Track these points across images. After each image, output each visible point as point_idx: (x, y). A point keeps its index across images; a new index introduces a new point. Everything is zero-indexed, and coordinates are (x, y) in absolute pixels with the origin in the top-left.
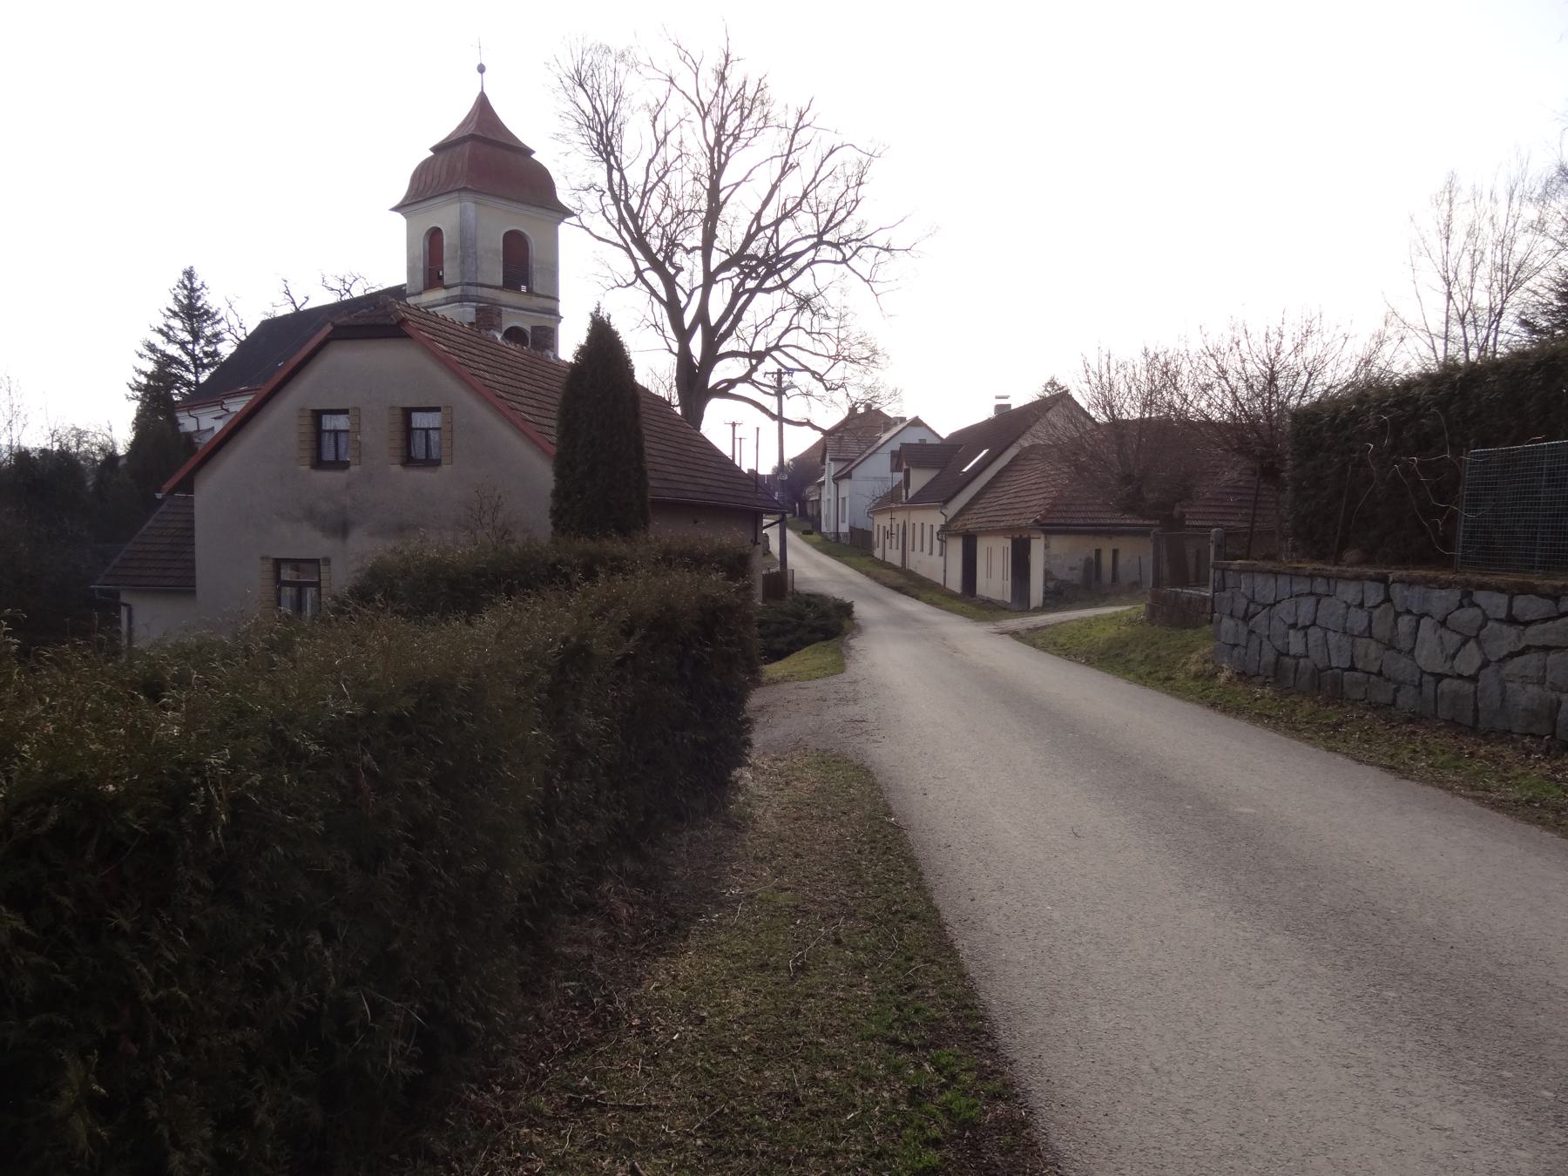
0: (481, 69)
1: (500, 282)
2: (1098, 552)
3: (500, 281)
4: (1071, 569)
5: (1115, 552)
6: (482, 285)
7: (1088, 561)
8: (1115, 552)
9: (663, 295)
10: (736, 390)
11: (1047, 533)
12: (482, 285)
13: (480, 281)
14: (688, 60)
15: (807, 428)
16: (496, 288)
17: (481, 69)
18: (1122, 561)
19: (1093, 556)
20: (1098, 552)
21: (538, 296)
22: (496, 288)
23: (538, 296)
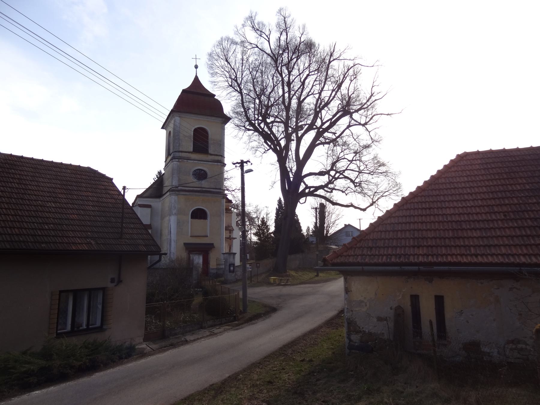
0: (196, 67)
1: (192, 150)
2: (415, 299)
3: (191, 149)
4: (380, 319)
5: (439, 300)
6: (182, 152)
7: (399, 312)
8: (439, 300)
9: (301, 156)
10: (318, 193)
11: (346, 274)
12: (182, 152)
13: (181, 150)
14: (264, 35)
15: (351, 208)
16: (189, 152)
17: (196, 67)
18: (449, 314)
19: (407, 306)
20: (415, 299)
21: (211, 155)
22: (189, 152)
23: (211, 155)
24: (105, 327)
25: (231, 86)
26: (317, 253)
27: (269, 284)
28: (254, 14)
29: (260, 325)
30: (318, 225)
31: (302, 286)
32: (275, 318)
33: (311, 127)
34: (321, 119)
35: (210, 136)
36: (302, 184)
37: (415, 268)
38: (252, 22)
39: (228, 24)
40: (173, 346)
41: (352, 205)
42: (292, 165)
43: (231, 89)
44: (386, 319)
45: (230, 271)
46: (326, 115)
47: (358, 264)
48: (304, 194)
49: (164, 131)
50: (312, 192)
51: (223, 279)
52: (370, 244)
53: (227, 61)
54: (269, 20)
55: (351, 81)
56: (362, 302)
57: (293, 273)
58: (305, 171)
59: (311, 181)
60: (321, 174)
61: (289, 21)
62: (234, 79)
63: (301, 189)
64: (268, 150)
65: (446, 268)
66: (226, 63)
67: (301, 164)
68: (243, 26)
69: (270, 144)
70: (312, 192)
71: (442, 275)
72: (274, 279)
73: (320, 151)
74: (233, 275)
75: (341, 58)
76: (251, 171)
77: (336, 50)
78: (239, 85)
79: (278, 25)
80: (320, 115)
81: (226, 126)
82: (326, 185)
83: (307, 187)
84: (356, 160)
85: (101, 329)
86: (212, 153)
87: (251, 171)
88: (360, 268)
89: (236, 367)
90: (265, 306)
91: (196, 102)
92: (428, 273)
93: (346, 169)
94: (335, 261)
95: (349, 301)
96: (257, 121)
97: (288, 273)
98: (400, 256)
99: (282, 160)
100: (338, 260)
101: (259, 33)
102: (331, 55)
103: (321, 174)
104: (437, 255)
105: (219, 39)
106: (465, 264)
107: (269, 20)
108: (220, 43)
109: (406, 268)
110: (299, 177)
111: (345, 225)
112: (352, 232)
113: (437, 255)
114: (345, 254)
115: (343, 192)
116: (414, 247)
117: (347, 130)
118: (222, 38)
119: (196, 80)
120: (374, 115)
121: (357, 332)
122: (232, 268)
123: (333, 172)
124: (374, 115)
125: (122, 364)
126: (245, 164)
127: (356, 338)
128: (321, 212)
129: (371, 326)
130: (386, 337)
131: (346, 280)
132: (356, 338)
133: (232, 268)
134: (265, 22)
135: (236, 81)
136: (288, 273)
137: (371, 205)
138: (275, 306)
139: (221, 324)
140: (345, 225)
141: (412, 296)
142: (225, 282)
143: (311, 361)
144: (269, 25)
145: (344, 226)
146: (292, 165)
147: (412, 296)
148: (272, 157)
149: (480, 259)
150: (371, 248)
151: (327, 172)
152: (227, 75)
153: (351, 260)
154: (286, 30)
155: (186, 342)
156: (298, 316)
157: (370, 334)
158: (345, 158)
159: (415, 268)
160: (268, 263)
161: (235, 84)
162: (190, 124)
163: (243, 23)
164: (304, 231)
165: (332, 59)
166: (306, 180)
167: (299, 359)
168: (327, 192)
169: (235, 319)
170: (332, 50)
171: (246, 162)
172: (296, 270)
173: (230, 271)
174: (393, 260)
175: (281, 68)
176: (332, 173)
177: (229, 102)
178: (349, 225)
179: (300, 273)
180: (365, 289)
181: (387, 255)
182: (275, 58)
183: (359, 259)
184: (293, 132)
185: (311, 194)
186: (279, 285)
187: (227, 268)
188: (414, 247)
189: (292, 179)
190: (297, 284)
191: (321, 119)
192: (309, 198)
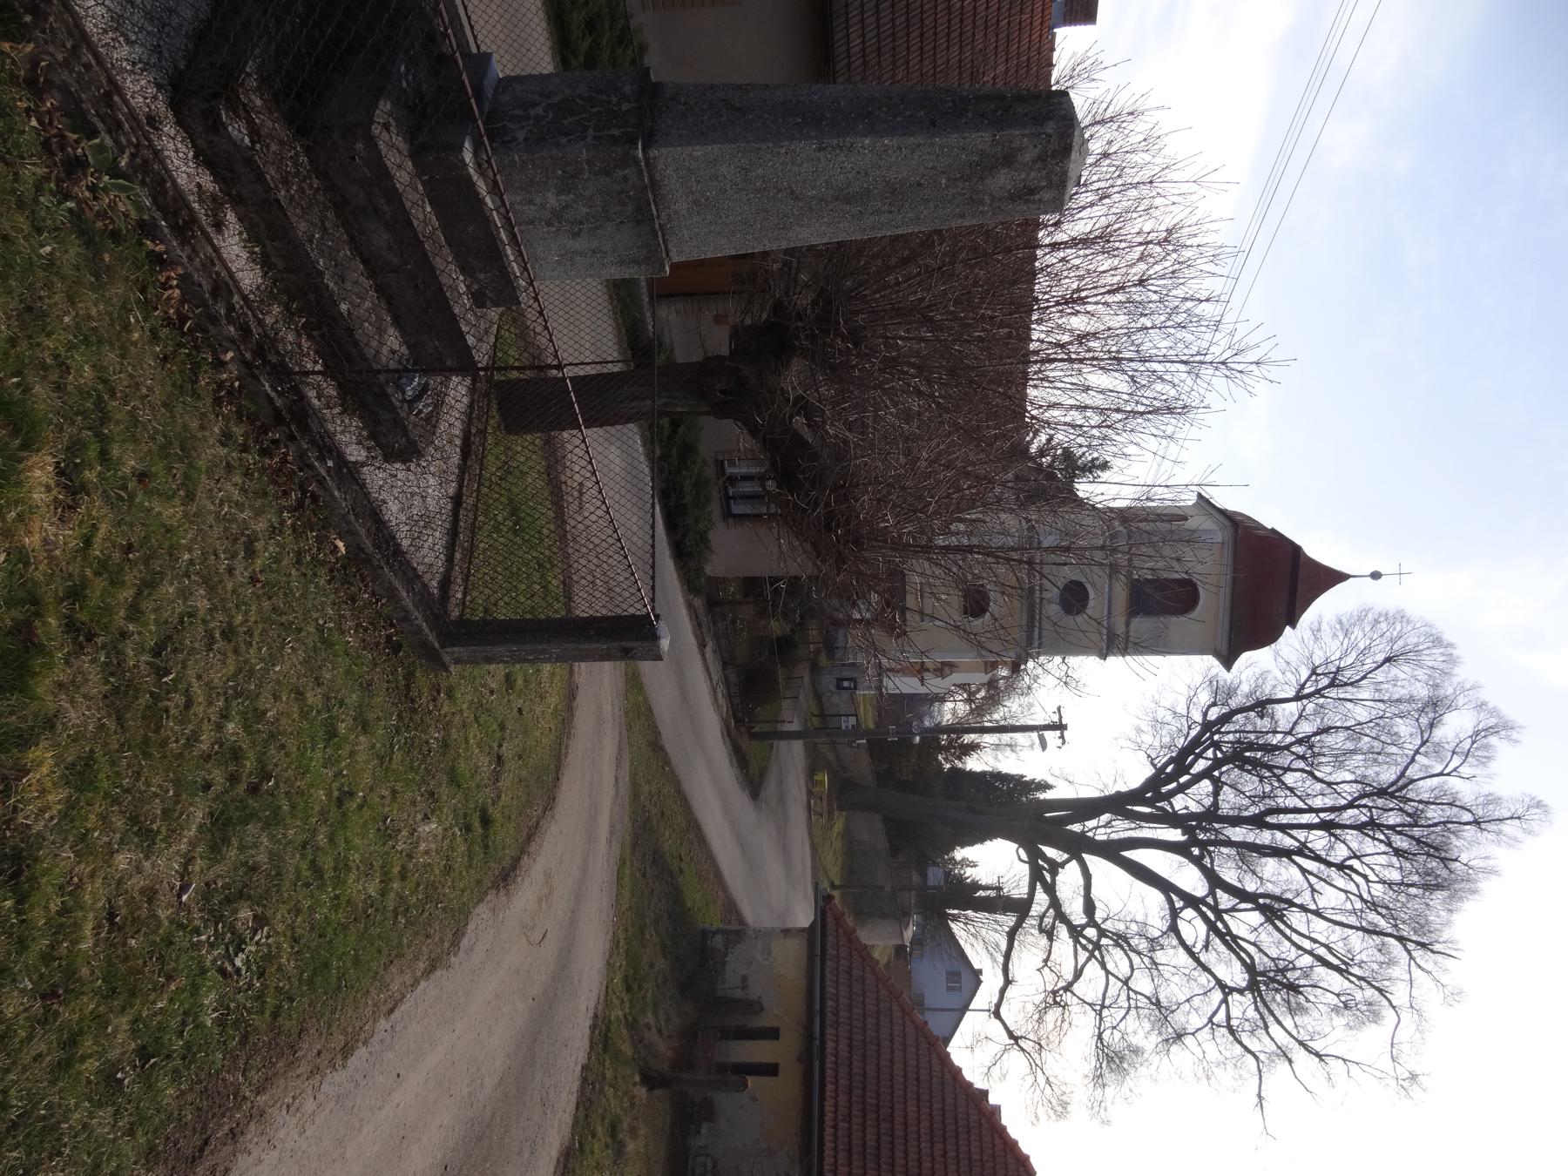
2: (772, 1034)
4: (745, 979)
5: (771, 1070)
7: (755, 1007)
8: (771, 1070)
17: (1376, 575)
19: (763, 1021)
20: (772, 1034)
21: (1127, 624)
23: (1127, 624)
24: (731, 520)
25: (1314, 672)
26: (888, 888)
27: (811, 772)
28: (1515, 735)
29: (727, 772)
30: (981, 893)
31: (808, 849)
32: (740, 799)
33: (1215, 881)
34: (1233, 909)
35: (1174, 619)
36: (1066, 856)
37: (817, 1034)
38: (1490, 730)
39: (1487, 670)
40: (698, 626)
41: (1008, 982)
42: (1101, 828)
43: (1305, 673)
44: (744, 988)
45: (840, 680)
46: (1246, 922)
47: (824, 949)
48: (1034, 857)
49: (1189, 499)
50: (1042, 874)
51: (823, 660)
52: (855, 972)
53: (1388, 660)
54: (1504, 776)
55: (1338, 995)
56: (770, 954)
57: (839, 826)
58: (1095, 862)
59: (1069, 880)
60: (1089, 907)
61: (1509, 828)
62: (1334, 679)
63: (1051, 852)
64: (1154, 766)
65: (817, 1078)
66: (1380, 658)
67: (1112, 851)
68: (1481, 706)
69: (1169, 770)
70: (1042, 874)
71: (807, 1078)
72: (822, 782)
73: (1149, 906)
74: (832, 688)
75: (1416, 972)
76: (1044, 745)
77: (1439, 958)
78: (1318, 692)
79: (1492, 800)
80: (1243, 906)
81: (1210, 657)
82: (1062, 917)
83: (1055, 867)
84: (1129, 998)
85: (728, 515)
86: (1132, 626)
87: (1044, 745)
88: (819, 951)
89: (675, 757)
90: (763, 773)
91: (1266, 582)
92: (811, 1053)
93: (1108, 972)
94: (829, 915)
95: (768, 934)
96: (1225, 744)
97: (836, 813)
98: (836, 1014)
99: (1118, 804)
100: (830, 919)
101: (1467, 745)
102: (1423, 945)
103: (1089, 907)
104: (836, 1070)
105: (1448, 637)
106: (822, 1107)
107: (1504, 776)
108: (1437, 641)
109: (817, 1021)
110: (1078, 847)
111: (980, 972)
112: (960, 989)
113: (836, 1070)
114: (841, 931)
115: (1046, 961)
116: (850, 1039)
117: (1213, 983)
118: (1450, 645)
119: (1331, 578)
120: (1256, 1058)
121: (726, 945)
122: (846, 684)
123: (1094, 935)
124: (1256, 1058)
125: (682, 584)
126: (1058, 733)
127: (718, 941)
128: (998, 902)
129: (735, 966)
130: (720, 986)
131: (803, 930)
132: (718, 941)
133: (846, 684)
134: (1494, 766)
135: (1332, 685)
136: (836, 813)
137: (1011, 1035)
138: (762, 795)
139: (729, 697)
140: (980, 972)
141: (777, 1030)
142: (815, 669)
143: (681, 871)
144: (1489, 776)
145: (976, 966)
146: (1101, 828)
147: (777, 1030)
148: (1136, 774)
149: (829, 1131)
150: (849, 972)
151: (1092, 922)
152: (1349, 660)
153: (831, 939)
154: (1476, 822)
155: (702, 646)
156: (742, 843)
157: (724, 964)
158: (1133, 970)
159: (817, 1034)
160: (862, 767)
161: (1329, 681)
162: (1210, 570)
163: (1490, 706)
164: (959, 854)
165: (1411, 946)
166: (1074, 865)
167: (683, 852)
168: (1042, 917)
169: (739, 721)
170: (1437, 947)
171: (1062, 737)
172: (847, 836)
173: (840, 680)
174: (830, 1003)
175: (1365, 806)
176: (1091, 932)
177: (1266, 667)
178: (979, 982)
179: (838, 844)
180: (788, 959)
181: (837, 995)
182: (1393, 792)
183: (831, 952)
184: (1199, 836)
185: (1036, 876)
186: (810, 794)
187: (847, 674)
188: (850, 1039)
189: (1076, 828)
190: (811, 837)
191: (1233, 909)
192: (1025, 869)
